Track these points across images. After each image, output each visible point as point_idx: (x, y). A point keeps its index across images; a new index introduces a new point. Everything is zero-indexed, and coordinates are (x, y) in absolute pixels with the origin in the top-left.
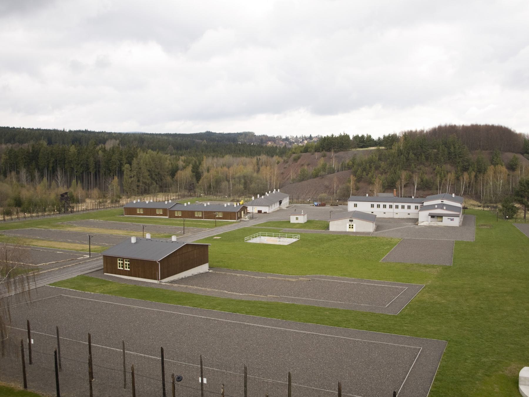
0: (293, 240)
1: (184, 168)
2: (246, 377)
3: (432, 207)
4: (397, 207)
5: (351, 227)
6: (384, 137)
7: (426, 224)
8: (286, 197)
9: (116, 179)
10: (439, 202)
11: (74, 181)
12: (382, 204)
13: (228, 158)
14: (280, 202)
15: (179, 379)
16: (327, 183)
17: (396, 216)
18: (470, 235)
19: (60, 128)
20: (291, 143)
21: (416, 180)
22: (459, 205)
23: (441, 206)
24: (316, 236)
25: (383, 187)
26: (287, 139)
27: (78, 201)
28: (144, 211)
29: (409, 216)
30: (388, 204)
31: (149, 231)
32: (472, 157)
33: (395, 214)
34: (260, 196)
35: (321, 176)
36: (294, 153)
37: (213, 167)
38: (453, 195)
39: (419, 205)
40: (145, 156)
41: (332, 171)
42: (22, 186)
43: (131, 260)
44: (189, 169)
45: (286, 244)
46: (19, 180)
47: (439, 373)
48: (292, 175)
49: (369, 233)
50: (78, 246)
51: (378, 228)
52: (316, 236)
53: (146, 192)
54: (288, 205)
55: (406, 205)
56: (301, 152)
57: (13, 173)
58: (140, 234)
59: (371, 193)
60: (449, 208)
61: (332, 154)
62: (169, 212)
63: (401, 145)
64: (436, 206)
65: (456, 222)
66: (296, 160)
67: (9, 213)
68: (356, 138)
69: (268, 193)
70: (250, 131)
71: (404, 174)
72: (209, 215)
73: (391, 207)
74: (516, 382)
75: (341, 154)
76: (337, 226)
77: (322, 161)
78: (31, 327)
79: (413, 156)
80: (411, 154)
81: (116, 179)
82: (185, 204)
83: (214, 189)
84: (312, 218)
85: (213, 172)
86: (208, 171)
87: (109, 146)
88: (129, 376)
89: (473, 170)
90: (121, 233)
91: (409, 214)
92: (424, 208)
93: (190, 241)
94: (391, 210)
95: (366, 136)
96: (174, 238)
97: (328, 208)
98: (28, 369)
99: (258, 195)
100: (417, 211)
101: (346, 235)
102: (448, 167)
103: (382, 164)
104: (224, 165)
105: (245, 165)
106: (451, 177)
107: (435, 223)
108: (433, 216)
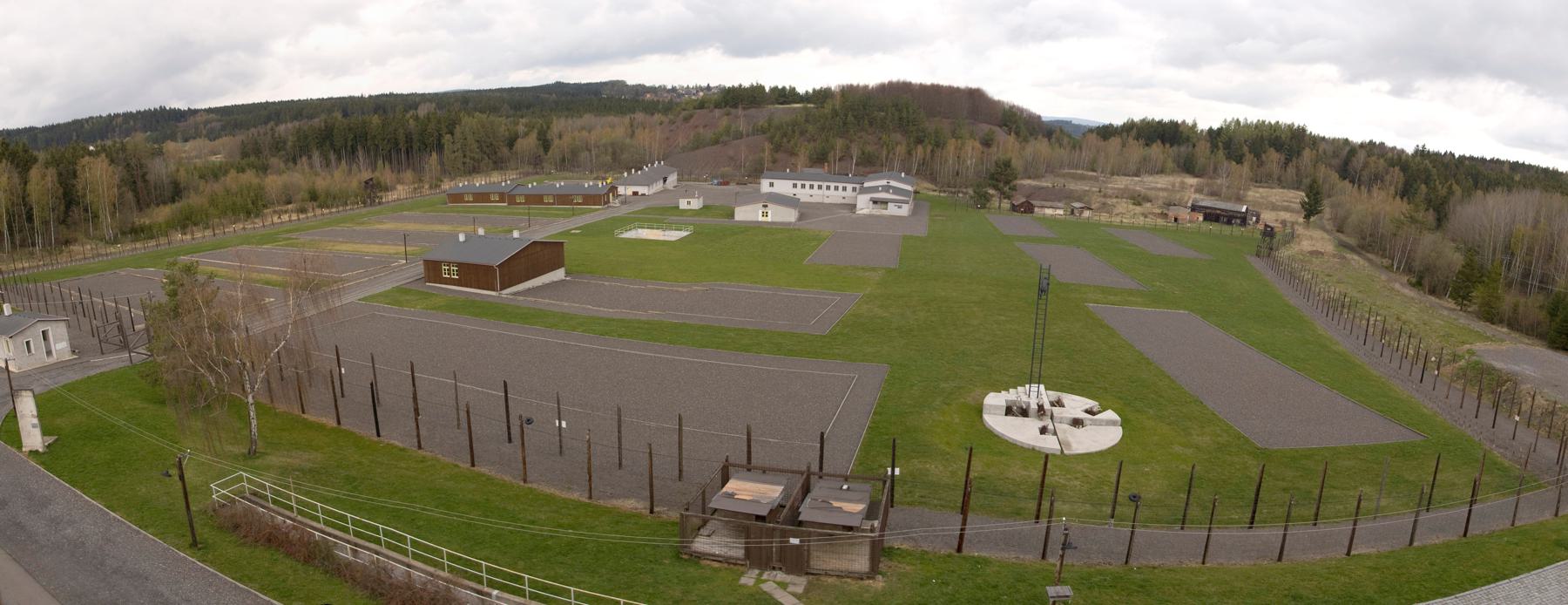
1: (526, 134)
2: (619, 420)
3: (875, 189)
5: (765, 214)
7: (865, 211)
9: (434, 155)
10: (884, 182)
11: (380, 162)
12: (807, 184)
13: (588, 118)
15: (529, 421)
16: (731, 153)
17: (827, 201)
18: (921, 229)
19: (357, 94)
20: (680, 95)
21: (855, 152)
22: (909, 188)
23: (887, 189)
24: (715, 229)
25: (811, 159)
26: (674, 89)
27: (387, 189)
30: (816, 184)
31: (482, 224)
32: (930, 125)
37: (566, 129)
40: (470, 122)
41: (738, 136)
42: (317, 174)
43: (459, 265)
44: (534, 135)
46: (311, 166)
47: (879, 405)
48: (681, 141)
50: (391, 249)
51: (801, 217)
52: (715, 229)
53: (474, 170)
55: (841, 186)
57: (304, 159)
58: (470, 228)
59: (794, 168)
60: (897, 191)
61: (740, 112)
62: (508, 197)
63: (838, 103)
65: (905, 211)
66: (686, 119)
67: (303, 210)
68: (774, 90)
71: (839, 143)
72: (563, 199)
74: (979, 410)
75: (752, 111)
76: (744, 214)
77: (725, 121)
81: (434, 155)
83: (568, 163)
84: (710, 202)
85: (567, 139)
86: (560, 137)
87: (422, 111)
88: (463, 414)
90: (445, 228)
92: (864, 191)
93: (538, 237)
96: (516, 234)
97: (733, 187)
98: (340, 401)
101: (756, 226)
102: (898, 136)
103: (810, 128)
104: (583, 128)
105: (613, 126)
106: (901, 150)
107: (878, 211)
108: (875, 202)
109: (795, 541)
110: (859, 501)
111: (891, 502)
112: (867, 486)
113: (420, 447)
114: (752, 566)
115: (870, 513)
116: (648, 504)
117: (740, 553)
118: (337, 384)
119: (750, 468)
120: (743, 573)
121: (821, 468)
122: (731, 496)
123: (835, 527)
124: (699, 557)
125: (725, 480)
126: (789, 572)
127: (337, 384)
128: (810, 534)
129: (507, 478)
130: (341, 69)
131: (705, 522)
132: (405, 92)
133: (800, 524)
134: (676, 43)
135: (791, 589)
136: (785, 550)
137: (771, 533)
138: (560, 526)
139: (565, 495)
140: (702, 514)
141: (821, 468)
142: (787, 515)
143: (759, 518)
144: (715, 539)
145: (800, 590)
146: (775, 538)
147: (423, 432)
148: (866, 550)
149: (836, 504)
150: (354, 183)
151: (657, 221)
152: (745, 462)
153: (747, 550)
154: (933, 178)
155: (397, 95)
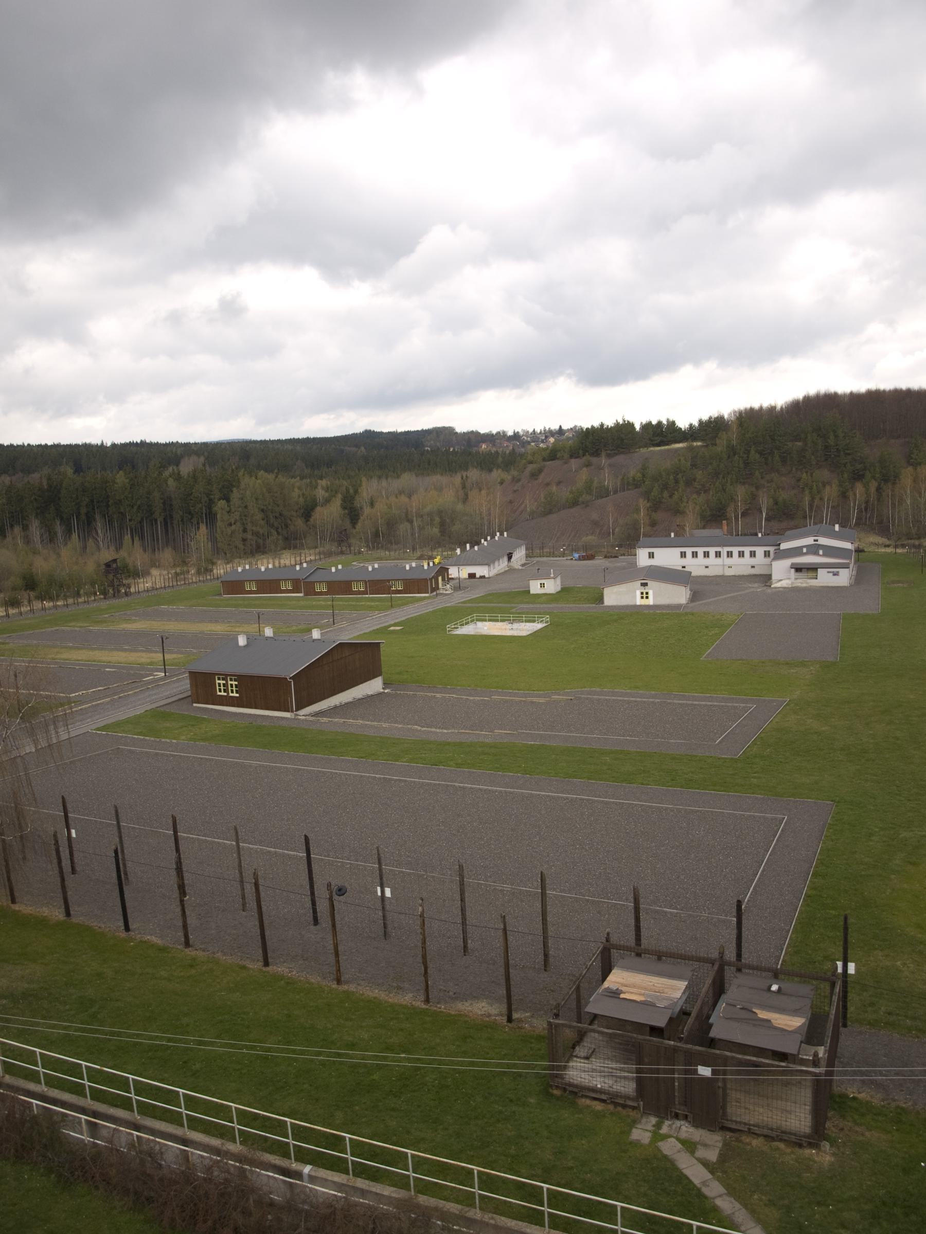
0: (538, 626)
1: (327, 501)
3: (797, 552)
4: (730, 554)
6: (700, 422)
7: (785, 583)
8: (520, 546)
9: (203, 528)
10: (809, 541)
11: (127, 538)
12: (700, 551)
13: (407, 479)
14: (510, 557)
15: (341, 891)
16: (595, 516)
17: (729, 572)
19: (95, 440)
20: (524, 444)
21: (765, 502)
22: (848, 545)
23: (814, 549)
24: (580, 620)
25: (703, 517)
26: (516, 436)
27: (136, 574)
28: (329, 588)
29: (753, 571)
30: (712, 551)
33: (726, 568)
34: (472, 547)
35: (583, 503)
36: (531, 462)
37: (379, 494)
38: (837, 527)
39: (772, 549)
41: (604, 493)
42: (35, 552)
43: (240, 678)
44: (337, 502)
45: (524, 634)
46: (27, 541)
48: (529, 504)
49: (679, 606)
50: (143, 658)
51: (695, 596)
52: (580, 620)
53: (259, 549)
54: (524, 561)
55: (747, 550)
56: (544, 460)
57: (17, 529)
60: (830, 551)
61: (603, 460)
62: (304, 585)
63: (734, 437)
64: (805, 550)
65: (844, 578)
66: (534, 475)
68: (647, 426)
69: (486, 540)
70: (447, 425)
71: (741, 492)
72: (378, 586)
73: (718, 554)
75: (620, 459)
76: (615, 596)
77: (584, 475)
78: (69, 806)
79: (757, 456)
80: (753, 452)
81: (203, 528)
82: (333, 570)
83: (384, 538)
85: (380, 506)
86: (372, 504)
87: (186, 467)
88: (249, 888)
89: (874, 477)
90: (219, 628)
91: (753, 567)
92: (781, 555)
93: (346, 638)
94: (719, 561)
95: (665, 422)
96: (316, 634)
97: (600, 562)
98: (70, 880)
99: (468, 545)
100: (767, 560)
103: (699, 474)
105: (440, 489)
106: (831, 492)
108: (798, 569)
109: (705, 1071)
110: (795, 1012)
111: (843, 1018)
112: (806, 989)
113: (187, 944)
114: (646, 1113)
115: (812, 1035)
116: (504, 1008)
117: (628, 1087)
118: (65, 853)
119: (641, 953)
120: (635, 1122)
121: (739, 955)
122: (615, 994)
123: (761, 1052)
124: (576, 1092)
125: (606, 970)
126: (697, 1124)
127: (65, 853)
128: (725, 1061)
129: (315, 979)
130: (65, 404)
131: (582, 1035)
132: (162, 440)
133: (712, 1043)
134: (516, 373)
135: (701, 1153)
136: (693, 1084)
137: (671, 1056)
138: (389, 1048)
139: (394, 999)
140: (577, 1021)
141: (739, 955)
142: (689, 1029)
143: (655, 1031)
144: (596, 1063)
145: (712, 1156)
146: (679, 1064)
147: (192, 921)
148: (806, 1095)
149: (762, 1014)
150: (90, 566)
151: (502, 611)
152: (632, 942)
153: (639, 1081)
154: (883, 528)
155: (151, 445)
